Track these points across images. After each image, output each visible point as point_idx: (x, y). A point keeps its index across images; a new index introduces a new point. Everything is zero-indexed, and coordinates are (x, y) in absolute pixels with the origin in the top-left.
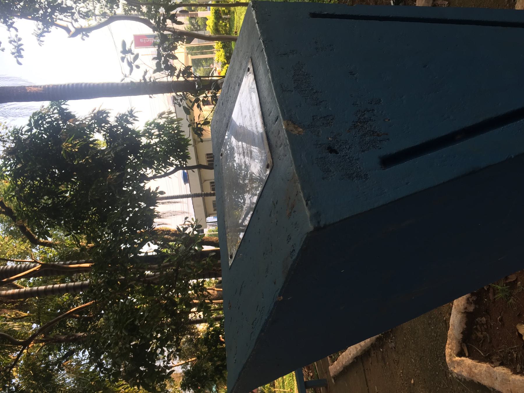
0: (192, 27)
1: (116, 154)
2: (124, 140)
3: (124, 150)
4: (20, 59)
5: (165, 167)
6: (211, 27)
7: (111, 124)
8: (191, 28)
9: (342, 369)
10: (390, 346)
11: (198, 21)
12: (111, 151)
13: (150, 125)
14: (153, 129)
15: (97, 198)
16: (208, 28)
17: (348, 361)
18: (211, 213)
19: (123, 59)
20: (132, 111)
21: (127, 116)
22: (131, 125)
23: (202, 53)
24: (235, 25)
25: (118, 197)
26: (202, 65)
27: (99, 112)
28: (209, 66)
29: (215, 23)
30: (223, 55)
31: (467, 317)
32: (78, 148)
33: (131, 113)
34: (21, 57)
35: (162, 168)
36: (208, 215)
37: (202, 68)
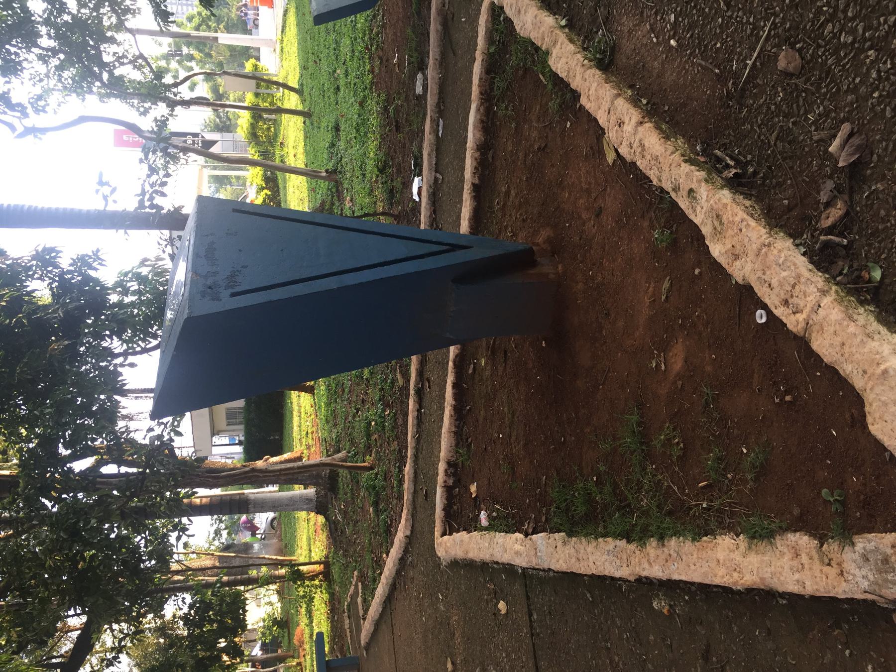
0: (218, 120)
1: (66, 313)
2: (82, 292)
3: (81, 308)
5: (144, 340)
6: (245, 129)
7: (63, 269)
8: (215, 121)
12: (58, 308)
13: (126, 274)
14: (129, 281)
15: (29, 377)
19: (97, 191)
20: (98, 251)
21: (90, 257)
22: (94, 271)
24: (282, 133)
25: (67, 367)
26: (231, 182)
27: (45, 249)
28: (242, 186)
29: (252, 124)
30: (260, 174)
32: (6, 301)
33: (96, 255)
35: (138, 340)
36: (215, 432)
37: (229, 187)
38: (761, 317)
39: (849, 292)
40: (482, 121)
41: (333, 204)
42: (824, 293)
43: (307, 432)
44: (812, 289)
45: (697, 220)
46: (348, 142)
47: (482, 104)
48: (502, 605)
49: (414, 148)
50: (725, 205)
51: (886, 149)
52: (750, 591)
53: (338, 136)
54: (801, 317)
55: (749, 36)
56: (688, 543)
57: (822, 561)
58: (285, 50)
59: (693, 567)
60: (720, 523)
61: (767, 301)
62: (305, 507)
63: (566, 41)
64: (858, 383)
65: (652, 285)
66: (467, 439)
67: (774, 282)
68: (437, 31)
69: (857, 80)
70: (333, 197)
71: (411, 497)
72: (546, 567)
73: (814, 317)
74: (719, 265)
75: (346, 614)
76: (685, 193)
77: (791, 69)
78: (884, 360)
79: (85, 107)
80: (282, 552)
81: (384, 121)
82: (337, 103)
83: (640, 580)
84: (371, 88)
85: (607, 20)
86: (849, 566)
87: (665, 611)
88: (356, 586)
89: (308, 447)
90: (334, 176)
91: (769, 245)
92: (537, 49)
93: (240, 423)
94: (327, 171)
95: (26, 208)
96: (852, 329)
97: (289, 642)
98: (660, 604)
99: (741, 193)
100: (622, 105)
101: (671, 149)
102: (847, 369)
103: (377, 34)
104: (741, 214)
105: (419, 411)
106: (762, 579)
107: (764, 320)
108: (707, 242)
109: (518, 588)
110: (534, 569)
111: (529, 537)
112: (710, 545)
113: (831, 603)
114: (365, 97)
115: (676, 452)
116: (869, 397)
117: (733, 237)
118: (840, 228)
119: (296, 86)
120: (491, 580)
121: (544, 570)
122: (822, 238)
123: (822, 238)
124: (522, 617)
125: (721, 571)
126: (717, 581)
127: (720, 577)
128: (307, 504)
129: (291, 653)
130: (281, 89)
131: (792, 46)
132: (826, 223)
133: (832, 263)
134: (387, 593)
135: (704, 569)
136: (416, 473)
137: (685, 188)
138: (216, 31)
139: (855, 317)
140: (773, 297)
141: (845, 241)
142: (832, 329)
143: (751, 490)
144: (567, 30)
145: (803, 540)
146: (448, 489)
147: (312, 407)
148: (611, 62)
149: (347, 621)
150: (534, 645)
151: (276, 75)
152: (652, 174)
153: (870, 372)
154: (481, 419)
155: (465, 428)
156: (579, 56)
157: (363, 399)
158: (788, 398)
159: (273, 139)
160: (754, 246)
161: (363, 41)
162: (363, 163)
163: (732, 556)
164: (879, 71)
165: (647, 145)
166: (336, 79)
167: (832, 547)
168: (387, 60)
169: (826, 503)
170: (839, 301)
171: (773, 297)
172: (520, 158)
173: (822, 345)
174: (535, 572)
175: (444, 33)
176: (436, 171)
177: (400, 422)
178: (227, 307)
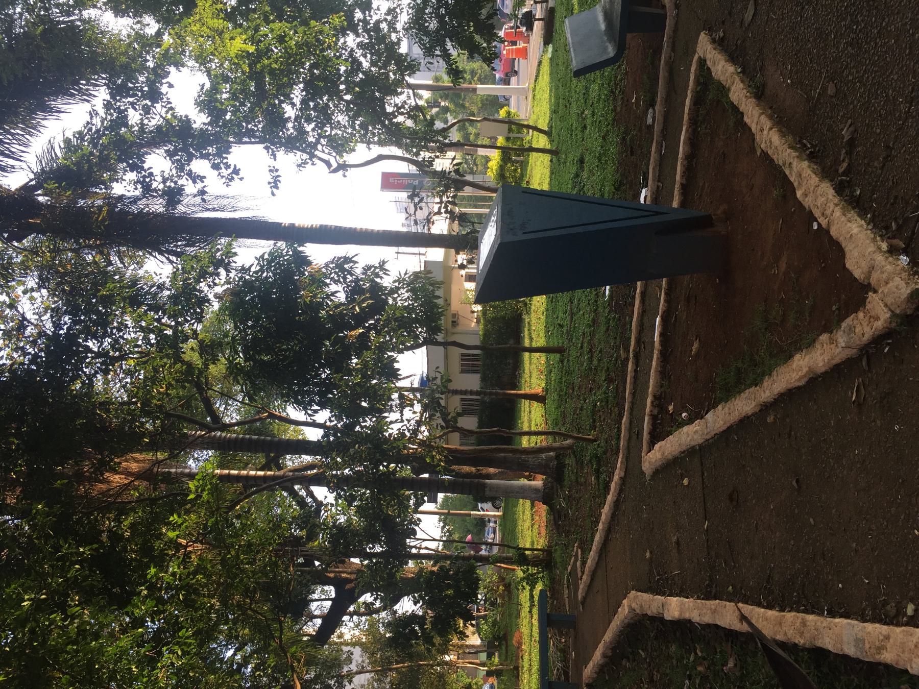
4: (275, 190)
11: (476, 159)
16: (489, 173)
20: (384, 262)
21: (376, 268)
23: (476, 207)
34: (277, 188)
40: (690, 139)
42: (836, 205)
45: (792, 180)
46: (591, 171)
47: (690, 126)
49: (644, 167)
50: (803, 169)
53: (582, 168)
58: (538, 97)
63: (739, 82)
71: (626, 444)
75: (566, 586)
81: (622, 148)
82: (583, 140)
84: (613, 124)
88: (577, 551)
92: (724, 87)
97: (507, 652)
101: (783, 141)
103: (621, 80)
105: (636, 371)
114: (608, 131)
118: (846, 173)
119: (546, 129)
128: (535, 493)
130: (531, 131)
132: (841, 170)
134: (603, 539)
136: (631, 423)
137: (788, 162)
138: (470, 83)
147: (542, 416)
148: (763, 93)
151: (527, 120)
152: (775, 157)
156: (745, 91)
157: (591, 388)
159: (519, 179)
161: (609, 86)
162: (603, 185)
166: (584, 119)
168: (628, 101)
177: (621, 389)
178: (521, 239)
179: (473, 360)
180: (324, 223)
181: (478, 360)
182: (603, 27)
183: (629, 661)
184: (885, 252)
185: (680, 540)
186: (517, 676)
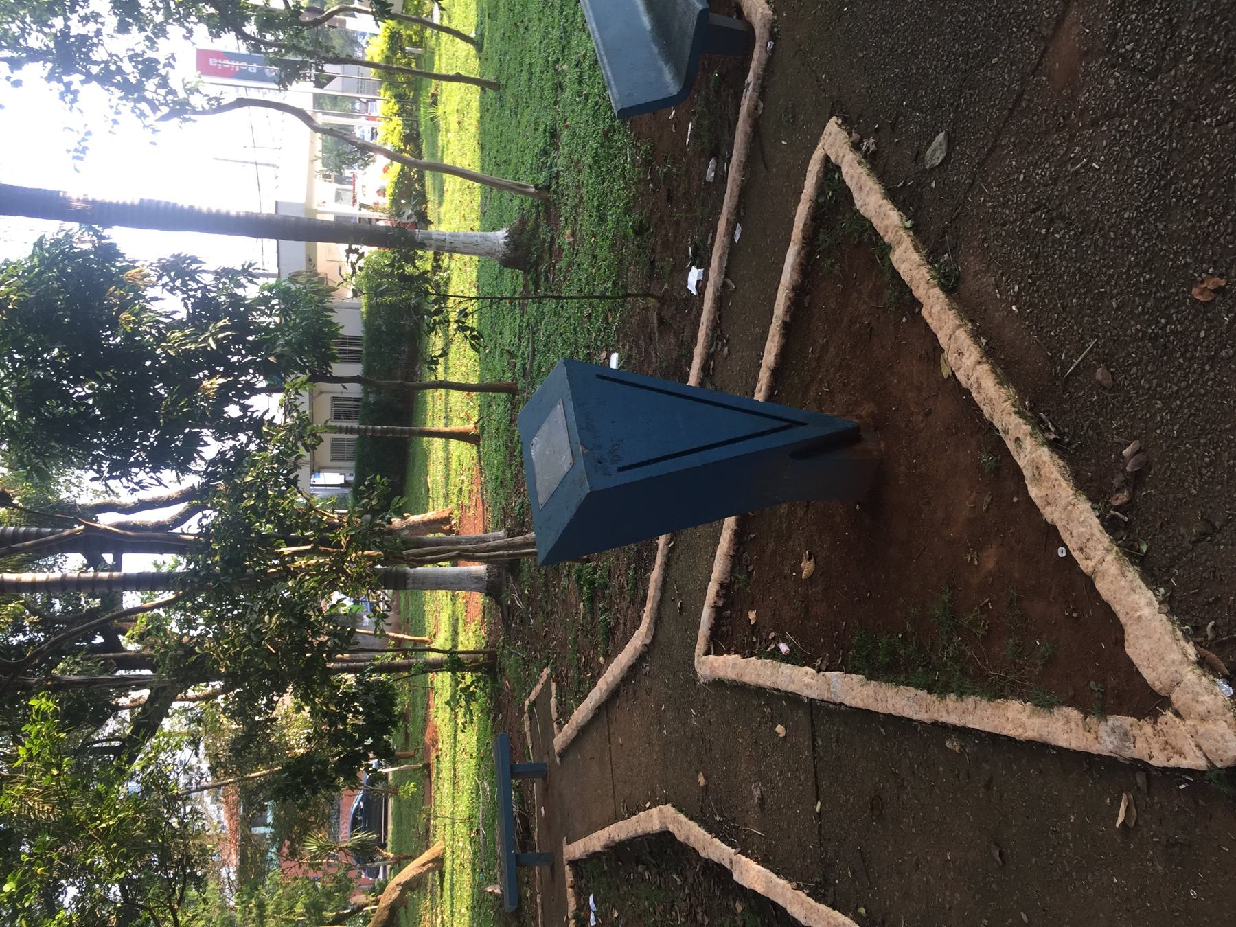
9: (575, 733)
10: (644, 672)
17: (586, 716)
18: (323, 464)
31: (716, 612)
38: (1062, 553)
39: (1125, 554)
40: (801, 264)
41: (537, 225)
42: (1108, 551)
43: (461, 489)
44: (1100, 547)
45: (1021, 463)
47: (803, 248)
48: (780, 729)
50: (1044, 462)
51: (1160, 470)
52: (1029, 742)
54: (1091, 564)
55: (1076, 342)
56: (984, 702)
57: (1085, 729)
59: (986, 720)
60: (1012, 691)
61: (1067, 543)
62: (473, 587)
64: (1123, 619)
65: (974, 494)
66: (747, 566)
67: (1074, 532)
68: (746, 133)
69: (1148, 415)
70: (538, 216)
72: (839, 701)
73: (1099, 566)
74: (1033, 504)
76: (1013, 439)
77: (1105, 383)
78: (1140, 609)
79: (194, 43)
80: (400, 628)
83: (935, 723)
85: (954, 249)
86: (1103, 734)
87: (957, 749)
89: (461, 507)
90: (545, 194)
91: (1074, 505)
93: (349, 459)
94: (536, 187)
95: (163, 204)
96: (1123, 583)
98: (952, 744)
99: (1057, 454)
100: (962, 335)
102: (1117, 608)
104: (1056, 474)
106: (1041, 735)
107: (1064, 555)
108: (1027, 482)
109: (801, 716)
110: (823, 701)
111: (821, 673)
112: (1003, 706)
113: (1088, 756)
115: (981, 632)
116: (1128, 630)
117: (1048, 488)
120: (768, 704)
121: (834, 703)
122: (1112, 512)
123: (1112, 512)
124: (804, 741)
125: (1010, 726)
126: (1005, 732)
127: (1009, 730)
129: (411, 752)
131: (1108, 368)
132: (1117, 503)
133: (1116, 530)
135: (995, 723)
136: (664, 581)
139: (1127, 574)
140: (1073, 542)
141: (1126, 519)
142: (1110, 579)
143: (1039, 672)
144: (911, 233)
145: (1074, 713)
146: (718, 611)
149: (527, 724)
150: (815, 767)
153: (1131, 614)
154: (769, 551)
155: (745, 555)
158: (1075, 615)
160: (1063, 502)
163: (1019, 716)
164: (1162, 417)
165: (983, 384)
167: (1092, 720)
169: (1092, 691)
170: (1118, 559)
171: (1073, 542)
172: (845, 321)
173: (1102, 586)
174: (823, 704)
175: (754, 137)
176: (726, 276)
179: (351, 345)
180: (147, 197)
181: (359, 345)
182: (646, 22)
183: (648, 869)
184: (1194, 663)
185: (765, 794)
186: (429, 776)
